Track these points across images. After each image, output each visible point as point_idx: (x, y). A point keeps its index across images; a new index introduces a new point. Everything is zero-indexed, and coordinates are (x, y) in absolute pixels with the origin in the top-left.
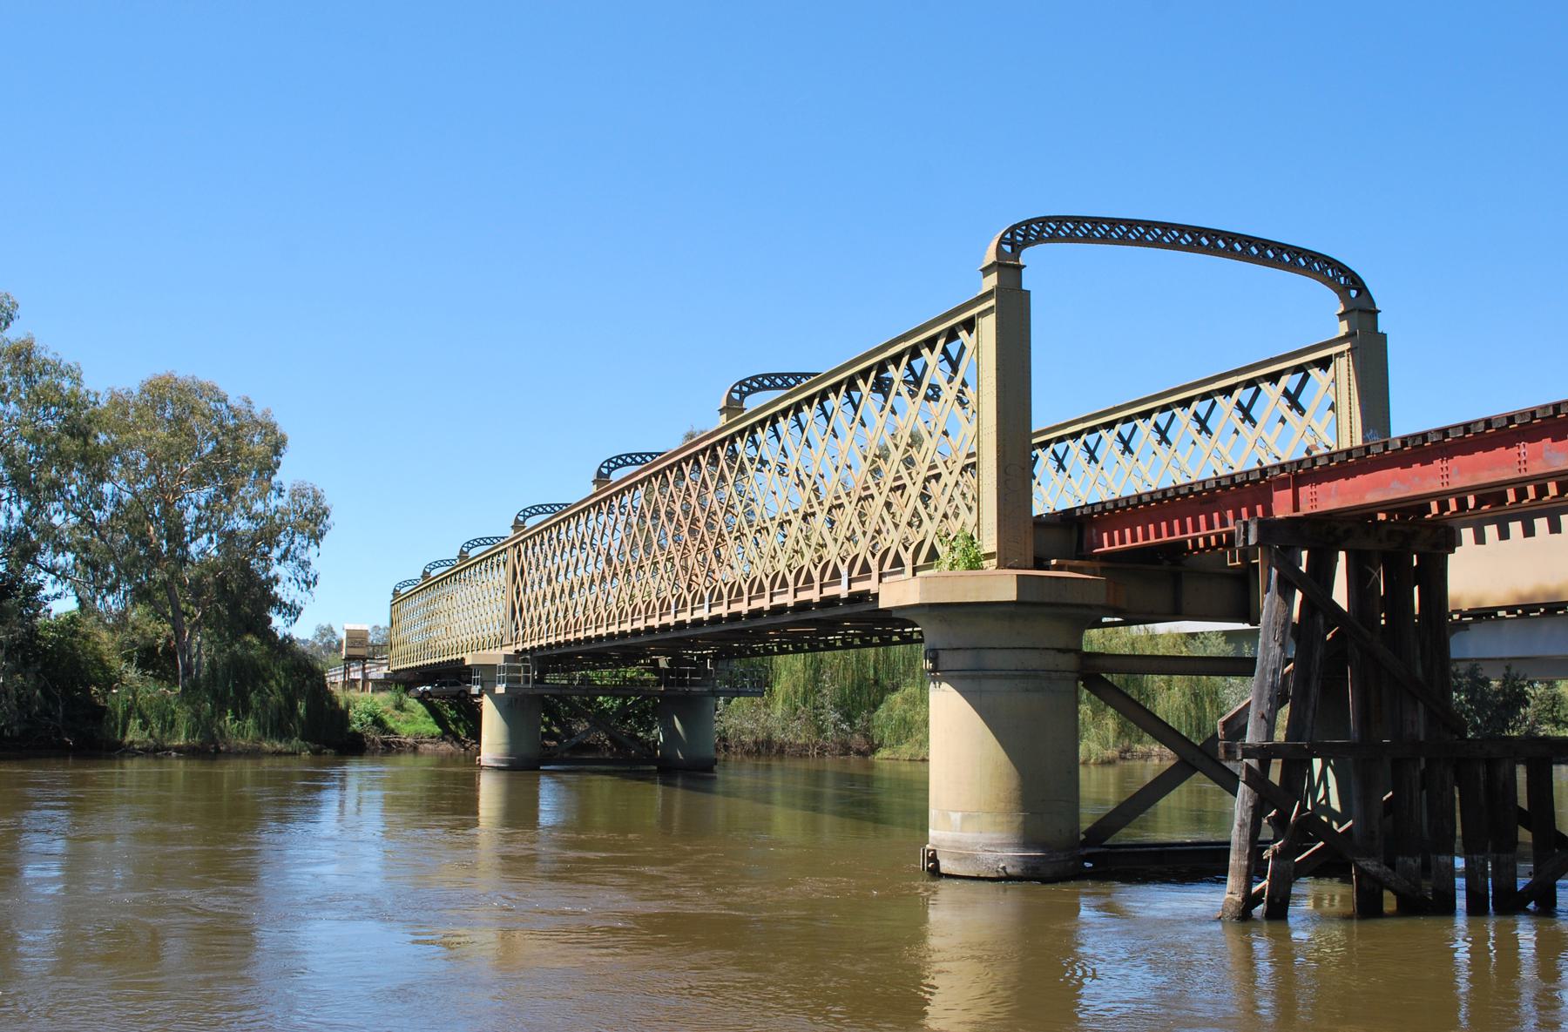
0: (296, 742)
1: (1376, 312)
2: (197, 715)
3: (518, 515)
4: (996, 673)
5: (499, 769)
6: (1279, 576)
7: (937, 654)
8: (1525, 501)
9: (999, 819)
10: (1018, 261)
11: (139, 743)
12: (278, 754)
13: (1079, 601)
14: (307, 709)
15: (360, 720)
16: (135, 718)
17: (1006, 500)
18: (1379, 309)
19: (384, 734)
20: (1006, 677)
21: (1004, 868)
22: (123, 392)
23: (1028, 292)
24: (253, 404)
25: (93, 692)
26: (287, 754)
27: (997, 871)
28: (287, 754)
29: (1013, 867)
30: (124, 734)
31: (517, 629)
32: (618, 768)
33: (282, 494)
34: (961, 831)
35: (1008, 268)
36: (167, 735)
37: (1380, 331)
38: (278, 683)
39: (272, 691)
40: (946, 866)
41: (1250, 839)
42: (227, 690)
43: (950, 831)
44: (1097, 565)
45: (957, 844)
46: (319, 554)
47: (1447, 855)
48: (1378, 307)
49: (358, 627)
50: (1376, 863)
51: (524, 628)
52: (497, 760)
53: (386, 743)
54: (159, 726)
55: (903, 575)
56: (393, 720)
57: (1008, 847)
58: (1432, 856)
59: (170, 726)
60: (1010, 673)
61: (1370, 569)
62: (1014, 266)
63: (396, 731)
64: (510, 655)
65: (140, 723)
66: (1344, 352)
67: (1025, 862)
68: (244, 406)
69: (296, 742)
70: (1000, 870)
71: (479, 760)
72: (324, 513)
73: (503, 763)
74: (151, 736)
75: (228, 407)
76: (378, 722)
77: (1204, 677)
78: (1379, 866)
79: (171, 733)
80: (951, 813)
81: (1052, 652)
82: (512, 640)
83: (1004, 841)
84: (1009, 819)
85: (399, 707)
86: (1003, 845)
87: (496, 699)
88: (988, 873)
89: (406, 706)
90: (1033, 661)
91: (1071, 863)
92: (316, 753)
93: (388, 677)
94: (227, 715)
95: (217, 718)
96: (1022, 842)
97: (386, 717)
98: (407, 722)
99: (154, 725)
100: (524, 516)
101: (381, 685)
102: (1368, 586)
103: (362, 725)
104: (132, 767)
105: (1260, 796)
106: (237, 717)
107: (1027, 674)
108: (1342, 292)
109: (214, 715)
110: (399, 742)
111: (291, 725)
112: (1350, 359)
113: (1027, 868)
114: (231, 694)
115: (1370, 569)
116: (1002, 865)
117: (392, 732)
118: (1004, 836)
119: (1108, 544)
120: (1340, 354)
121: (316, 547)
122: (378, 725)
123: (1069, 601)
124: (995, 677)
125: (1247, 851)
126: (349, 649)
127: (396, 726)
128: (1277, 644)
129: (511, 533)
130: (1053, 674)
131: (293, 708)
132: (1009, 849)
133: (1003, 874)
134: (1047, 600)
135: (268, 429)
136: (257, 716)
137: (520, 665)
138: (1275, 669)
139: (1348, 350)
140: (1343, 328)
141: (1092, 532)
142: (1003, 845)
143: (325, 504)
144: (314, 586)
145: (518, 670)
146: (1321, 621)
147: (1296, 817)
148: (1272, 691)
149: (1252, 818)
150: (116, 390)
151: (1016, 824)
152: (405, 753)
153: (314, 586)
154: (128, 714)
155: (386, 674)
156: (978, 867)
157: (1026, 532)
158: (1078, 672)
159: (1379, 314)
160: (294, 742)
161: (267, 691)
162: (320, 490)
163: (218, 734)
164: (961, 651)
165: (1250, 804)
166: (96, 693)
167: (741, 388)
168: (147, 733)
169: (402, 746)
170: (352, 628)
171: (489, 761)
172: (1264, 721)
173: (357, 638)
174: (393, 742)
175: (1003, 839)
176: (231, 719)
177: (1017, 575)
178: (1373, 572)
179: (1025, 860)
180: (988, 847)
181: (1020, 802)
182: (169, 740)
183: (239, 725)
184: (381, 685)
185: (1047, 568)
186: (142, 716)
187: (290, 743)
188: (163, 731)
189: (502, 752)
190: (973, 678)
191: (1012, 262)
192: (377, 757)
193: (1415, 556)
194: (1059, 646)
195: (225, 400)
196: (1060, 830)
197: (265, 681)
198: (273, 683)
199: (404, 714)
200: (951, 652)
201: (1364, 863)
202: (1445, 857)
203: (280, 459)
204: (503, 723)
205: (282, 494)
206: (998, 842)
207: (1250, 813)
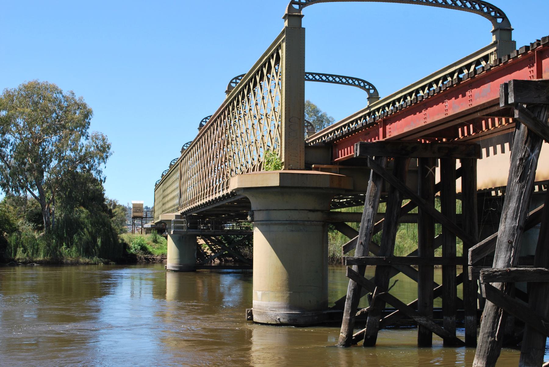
0: (96, 259)
1: (511, 30)
2: (49, 245)
4: (276, 222)
5: (175, 271)
6: (373, 172)
7: (253, 213)
9: (277, 295)
10: (300, 13)
11: (21, 259)
12: (87, 264)
13: (315, 186)
14: (102, 242)
15: (135, 248)
16: (20, 248)
17: (289, 135)
18: (513, 28)
19: (146, 255)
20: (281, 224)
21: (279, 319)
22: (13, 91)
23: (304, 29)
24: (75, 94)
25: (5, 235)
26: (91, 264)
27: (276, 321)
28: (91, 264)
29: (284, 318)
30: (15, 255)
32: (235, 271)
33: (88, 138)
34: (261, 301)
36: (35, 255)
37: (513, 40)
38: (88, 229)
39: (84, 234)
40: (256, 318)
41: (351, 306)
42: (63, 234)
43: (257, 301)
44: (338, 167)
45: (260, 307)
46: (105, 167)
47: (471, 316)
48: (512, 27)
49: (138, 202)
50: (425, 319)
52: (174, 267)
53: (146, 259)
54: (31, 251)
56: (151, 248)
57: (281, 309)
58: (465, 317)
59: (36, 251)
60: (283, 222)
61: (427, 167)
62: (297, 16)
63: (152, 253)
64: (178, 215)
65: (22, 250)
66: (493, 52)
67: (289, 316)
68: (71, 97)
69: (96, 259)
70: (277, 320)
71: (166, 267)
72: (108, 147)
73: (176, 268)
74: (27, 256)
75: (63, 96)
76: (144, 249)
78: (427, 321)
79: (37, 255)
80: (258, 292)
81: (306, 212)
83: (280, 306)
84: (282, 295)
85: (155, 241)
86: (279, 308)
87: (171, 236)
88: (271, 322)
89: (158, 241)
90: (295, 216)
91: (316, 318)
92: (106, 263)
93: (153, 226)
94: (63, 245)
95: (59, 247)
96: (288, 306)
97: (148, 246)
98: (158, 249)
99: (29, 251)
100: (187, 146)
101: (148, 231)
102: (427, 176)
103: (135, 250)
104: (19, 271)
105: (357, 284)
106: (68, 246)
107: (291, 223)
108: (493, 19)
109: (57, 246)
110: (154, 258)
111: (94, 250)
112: (496, 56)
113: (290, 320)
114: (65, 235)
115: (427, 167)
116: (278, 318)
117: (150, 253)
118: (280, 303)
119: (343, 154)
120: (492, 53)
121: (104, 163)
122: (143, 250)
123: (308, 186)
124: (276, 224)
125: (350, 312)
126: (135, 213)
127: (153, 250)
128: (371, 207)
130: (306, 222)
131: (95, 242)
132: (282, 310)
133: (279, 322)
134: (296, 185)
135: (81, 106)
136: (76, 245)
137: (183, 220)
138: (369, 220)
139: (495, 51)
140: (494, 39)
141: (336, 150)
142: (279, 308)
143: (108, 142)
144: (104, 183)
145: (182, 222)
146: (398, 195)
147: (375, 295)
148: (367, 230)
149: (353, 295)
150: (9, 90)
151: (285, 298)
152: (157, 263)
153: (104, 183)
154: (16, 246)
155: (152, 225)
156: (267, 318)
157: (300, 151)
158: (323, 221)
159: (513, 31)
160: (94, 259)
161: (82, 234)
162: (105, 136)
163: (59, 255)
164: (262, 211)
165: (352, 288)
166: (6, 236)
167: (236, 81)
168: (26, 254)
169: (155, 260)
170: (135, 203)
171: (170, 267)
172: (362, 246)
173: (138, 208)
174: (150, 258)
175: (279, 305)
176: (65, 248)
178: (429, 169)
179: (290, 315)
180: (272, 309)
181: (288, 286)
182: (36, 257)
183: (68, 251)
184: (148, 231)
185: (311, 169)
186: (23, 246)
187: (93, 259)
188: (33, 254)
189: (176, 263)
190: (267, 225)
191: (296, 14)
192: (142, 266)
193: (439, 160)
194: (309, 209)
195: (61, 93)
196: (310, 301)
197: (82, 229)
198: (85, 230)
199: (157, 245)
200: (258, 212)
201: (419, 319)
202: (470, 317)
203: (90, 121)
204: (178, 250)
205: (88, 138)
206: (277, 306)
207: (352, 293)
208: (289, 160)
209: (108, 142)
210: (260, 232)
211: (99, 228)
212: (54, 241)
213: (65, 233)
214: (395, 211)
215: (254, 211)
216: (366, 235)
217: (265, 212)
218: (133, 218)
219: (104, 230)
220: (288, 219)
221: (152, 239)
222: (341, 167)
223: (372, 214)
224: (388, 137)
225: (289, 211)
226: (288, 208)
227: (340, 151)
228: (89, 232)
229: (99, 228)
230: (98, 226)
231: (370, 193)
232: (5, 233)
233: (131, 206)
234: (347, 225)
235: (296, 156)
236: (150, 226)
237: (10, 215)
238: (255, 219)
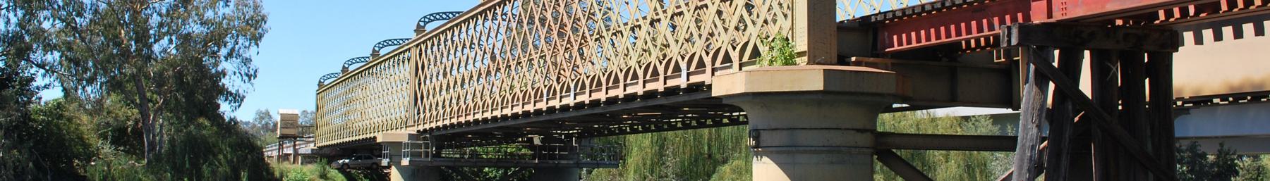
3: (420, 21)
6: (1036, 71)
7: (759, 134)
8: (1236, 10)
17: (815, 9)
20: (815, 152)
25: (75, 164)
31: (419, 113)
33: (229, 4)
38: (225, 157)
44: (889, 61)
46: (258, 53)
49: (290, 112)
51: (424, 112)
55: (731, 70)
61: (1109, 64)
64: (413, 135)
72: (263, 19)
77: (975, 152)
82: (415, 122)
89: (329, 175)
90: (837, 139)
93: (315, 152)
101: (309, 159)
107: (832, 150)
114: (187, 166)
115: (1109, 64)
123: (865, 91)
124: (805, 152)
128: (1035, 125)
129: (414, 36)
138: (1032, 146)
143: (264, 12)
145: (419, 146)
146: (1070, 107)
155: (312, 150)
158: (873, 148)
161: (217, 163)
164: (778, 131)
166: (78, 165)
170: (290, 113)
173: (289, 121)
177: (824, 70)
184: (309, 159)
185: (848, 64)
194: (858, 127)
197: (215, 156)
198: (221, 157)
200: (770, 132)
205: (229, 4)
208: (814, 48)
209: (264, 12)
210: (775, 165)
211: (244, 154)
212: (169, 174)
213: (187, 162)
214: (1067, 133)
215: (762, 131)
216: (1029, 171)
217: (785, 132)
218: (280, 138)
219: (252, 157)
220: (826, 145)
221: (317, 173)
222: (894, 61)
223: (1037, 137)
224: (1058, 16)
225: (827, 131)
226: (823, 127)
227: (895, 37)
228: (228, 162)
229: (244, 154)
230: (241, 150)
231: (1033, 103)
232: (76, 161)
233: (278, 119)
234: (895, 155)
235: (824, 44)
236: (310, 152)
237: (83, 128)
238: (762, 145)
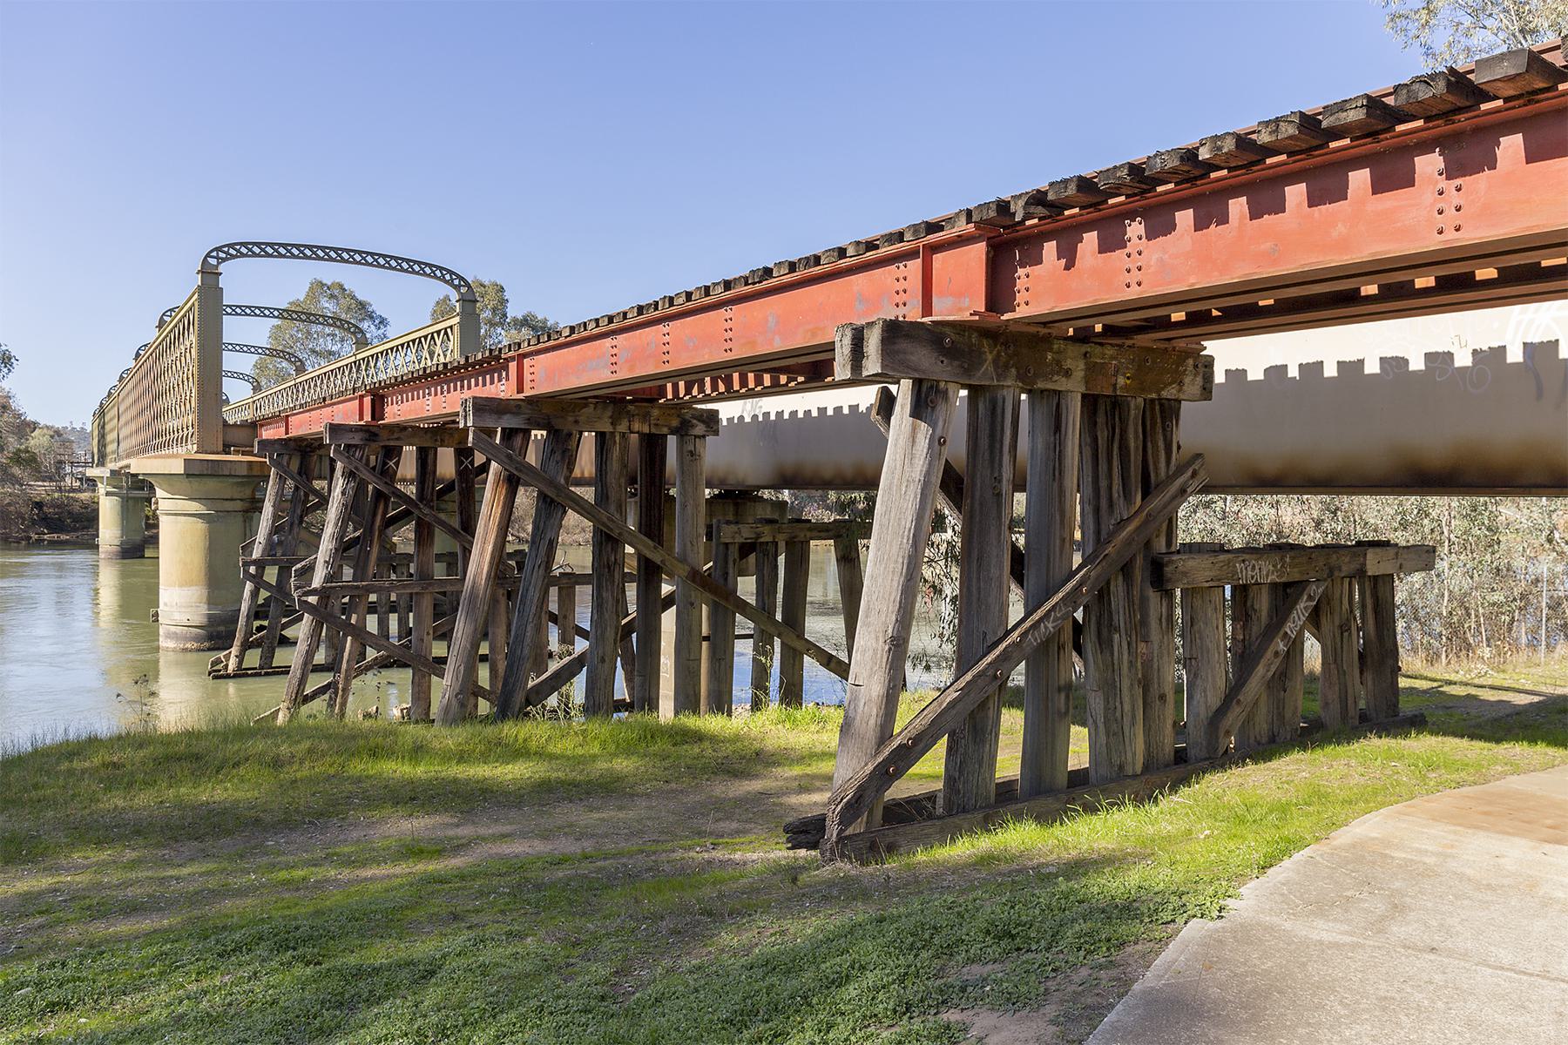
35: (209, 273)
